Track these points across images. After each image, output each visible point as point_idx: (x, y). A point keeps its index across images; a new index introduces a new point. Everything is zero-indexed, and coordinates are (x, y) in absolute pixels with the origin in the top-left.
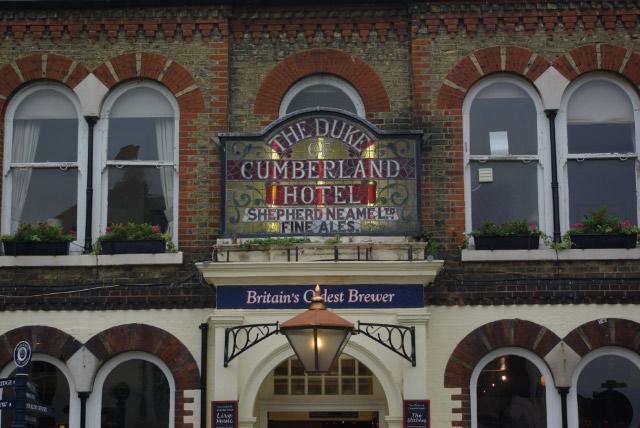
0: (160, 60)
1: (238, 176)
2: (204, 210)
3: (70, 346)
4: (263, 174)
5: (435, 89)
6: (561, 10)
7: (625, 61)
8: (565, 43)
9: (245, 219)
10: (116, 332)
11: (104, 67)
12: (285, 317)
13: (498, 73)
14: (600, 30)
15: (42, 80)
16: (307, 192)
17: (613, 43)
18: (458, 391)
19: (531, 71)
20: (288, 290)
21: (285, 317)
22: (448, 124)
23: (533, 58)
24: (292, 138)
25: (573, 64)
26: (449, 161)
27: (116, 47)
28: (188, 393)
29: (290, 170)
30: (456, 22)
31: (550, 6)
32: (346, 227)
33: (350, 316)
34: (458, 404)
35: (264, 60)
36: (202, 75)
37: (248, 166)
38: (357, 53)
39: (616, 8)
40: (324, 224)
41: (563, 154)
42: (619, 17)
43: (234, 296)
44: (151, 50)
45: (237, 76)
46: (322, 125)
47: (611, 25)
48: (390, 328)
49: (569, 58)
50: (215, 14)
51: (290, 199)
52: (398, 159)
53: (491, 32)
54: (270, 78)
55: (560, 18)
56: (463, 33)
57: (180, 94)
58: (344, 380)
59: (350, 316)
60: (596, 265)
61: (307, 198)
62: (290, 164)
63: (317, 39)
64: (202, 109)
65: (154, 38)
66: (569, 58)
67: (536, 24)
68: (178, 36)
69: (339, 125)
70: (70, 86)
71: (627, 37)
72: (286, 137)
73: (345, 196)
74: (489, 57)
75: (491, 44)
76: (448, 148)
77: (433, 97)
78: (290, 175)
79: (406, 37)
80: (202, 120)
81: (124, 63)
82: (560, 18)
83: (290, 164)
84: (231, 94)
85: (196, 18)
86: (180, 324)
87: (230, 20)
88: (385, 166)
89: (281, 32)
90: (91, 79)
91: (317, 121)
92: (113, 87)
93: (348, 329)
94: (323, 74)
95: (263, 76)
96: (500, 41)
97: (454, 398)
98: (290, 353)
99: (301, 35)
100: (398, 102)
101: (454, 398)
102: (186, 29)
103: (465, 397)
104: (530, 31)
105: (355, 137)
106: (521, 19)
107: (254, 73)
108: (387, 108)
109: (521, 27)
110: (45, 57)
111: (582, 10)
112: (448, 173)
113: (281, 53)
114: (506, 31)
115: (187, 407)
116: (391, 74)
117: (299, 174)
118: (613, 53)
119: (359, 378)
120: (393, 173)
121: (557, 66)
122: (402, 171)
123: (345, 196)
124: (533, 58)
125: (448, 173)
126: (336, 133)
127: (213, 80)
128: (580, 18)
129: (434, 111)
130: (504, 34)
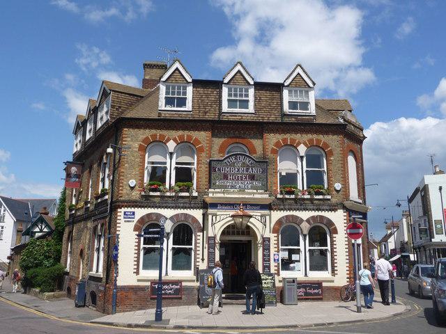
2: (204, 180)
10: (313, 217)
12: (232, 213)
13: (287, 145)
18: (276, 235)
20: (230, 205)
21: (232, 213)
28: (198, 234)
33: (251, 213)
34: (136, 255)
41: (305, 169)
43: (214, 206)
53: (285, 134)
54: (223, 143)
58: (176, 252)
59: (251, 213)
64: (203, 151)
73: (246, 178)
74: (285, 140)
75: (285, 137)
79: (262, 138)
80: (203, 155)
81: (181, 137)
84: (211, 148)
86: (197, 214)
91: (251, 109)
93: (251, 217)
96: (288, 136)
98: (233, 222)
115: (198, 245)
118: (319, 141)
119: (248, 231)
123: (246, 178)
129: (270, 155)
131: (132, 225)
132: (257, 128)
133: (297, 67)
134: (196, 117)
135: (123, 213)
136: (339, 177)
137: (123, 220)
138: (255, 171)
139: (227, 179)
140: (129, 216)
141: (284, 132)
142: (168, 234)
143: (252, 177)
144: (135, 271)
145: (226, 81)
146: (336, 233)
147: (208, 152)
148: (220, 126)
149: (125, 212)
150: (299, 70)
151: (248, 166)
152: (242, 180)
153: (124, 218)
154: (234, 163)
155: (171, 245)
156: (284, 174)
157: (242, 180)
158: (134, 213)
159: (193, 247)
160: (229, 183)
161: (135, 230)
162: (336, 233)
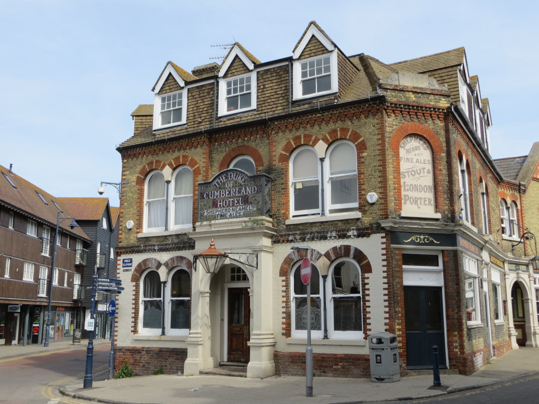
0: (299, 138)
1: (203, 198)
3: (159, 265)
4: (211, 196)
5: (278, 156)
6: (323, 116)
7: (349, 134)
8: (326, 129)
9: (205, 214)
11: (171, 162)
14: (339, 122)
15: (181, 165)
16: (226, 201)
17: (345, 126)
18: (284, 278)
19: (313, 143)
22: (282, 169)
23: (313, 138)
24: (221, 182)
25: (329, 138)
26: (282, 184)
27: (174, 154)
29: (220, 194)
30: (284, 127)
31: (318, 115)
32: (238, 215)
34: (367, 287)
35: (222, 152)
36: (200, 161)
37: (207, 194)
38: (253, 144)
39: (344, 112)
40: (231, 214)
42: (346, 115)
44: (185, 154)
45: (213, 160)
46: (231, 175)
47: (343, 119)
48: (248, 255)
49: (327, 135)
50: (203, 137)
51: (220, 205)
52: (256, 186)
53: (298, 129)
54: (224, 158)
55: (323, 119)
56: (288, 131)
57: (356, 143)
60: (336, 222)
61: (226, 204)
62: (220, 192)
63: (239, 141)
64: (200, 174)
65: (186, 149)
66: (327, 135)
67: (314, 123)
68: (280, 132)
69: (236, 175)
70: (313, 145)
71: (350, 123)
72: (219, 181)
75: (298, 134)
76: (282, 179)
77: (277, 158)
78: (220, 196)
79: (268, 136)
82: (323, 119)
83: (220, 192)
85: (197, 140)
87: (209, 139)
88: (252, 189)
89: (227, 140)
90: (321, 142)
92: (329, 145)
94: (243, 155)
95: (222, 158)
96: (301, 133)
97: (283, 281)
99: (234, 140)
100: (266, 163)
101: (283, 281)
102: (195, 144)
103: (287, 281)
104: (312, 126)
105: (242, 179)
106: (308, 122)
107: (219, 157)
108: (263, 165)
109: (309, 125)
110: (154, 161)
111: (331, 114)
112: (282, 189)
113: (227, 149)
114: (303, 128)
116: (263, 151)
117: (223, 195)
120: (254, 191)
121: (323, 140)
122: (257, 190)
123: (238, 202)
124: (313, 138)
125: (282, 189)
126: (235, 178)
127: (204, 162)
128: (331, 118)
129: (277, 164)
130: (303, 129)
131: (129, 275)
132: (260, 126)
133: (167, 64)
134: (191, 131)
135: (122, 261)
136: (375, 181)
137: (122, 269)
138: (249, 191)
139: (217, 207)
140: (127, 264)
141: (341, 118)
142: (165, 283)
143: (246, 200)
144: (133, 329)
145: (221, 74)
146: (369, 270)
147: (205, 174)
148: (217, 134)
149: (124, 260)
150: (313, 31)
151: (241, 185)
152: (233, 205)
153: (123, 267)
154: (224, 184)
155: (330, 295)
156: (299, 186)
157: (233, 205)
158: (131, 259)
159: (321, 295)
160: (217, 212)
161: (132, 281)
162: (369, 270)
